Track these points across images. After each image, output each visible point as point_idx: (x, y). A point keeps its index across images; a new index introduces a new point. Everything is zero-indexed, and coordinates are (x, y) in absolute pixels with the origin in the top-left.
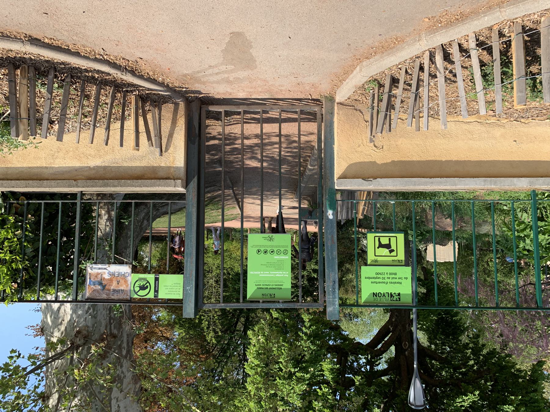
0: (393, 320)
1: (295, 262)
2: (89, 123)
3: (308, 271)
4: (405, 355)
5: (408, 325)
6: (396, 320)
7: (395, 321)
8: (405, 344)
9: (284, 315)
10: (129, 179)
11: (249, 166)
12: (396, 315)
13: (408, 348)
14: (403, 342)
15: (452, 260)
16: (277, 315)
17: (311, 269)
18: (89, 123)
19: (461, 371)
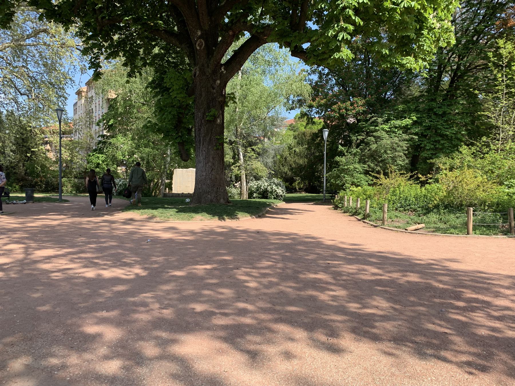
0: (218, 82)
1: (368, 165)
2: (509, 172)
3: (350, 153)
4: (201, 29)
5: (197, 75)
6: (215, 81)
7: (216, 80)
8: (200, 47)
9: (392, 63)
10: (61, 256)
11: (51, 243)
12: (214, 88)
13: (197, 41)
14: (204, 49)
15: (195, 169)
16: (404, 62)
17: (345, 156)
18: (509, 172)
19: (130, 17)
